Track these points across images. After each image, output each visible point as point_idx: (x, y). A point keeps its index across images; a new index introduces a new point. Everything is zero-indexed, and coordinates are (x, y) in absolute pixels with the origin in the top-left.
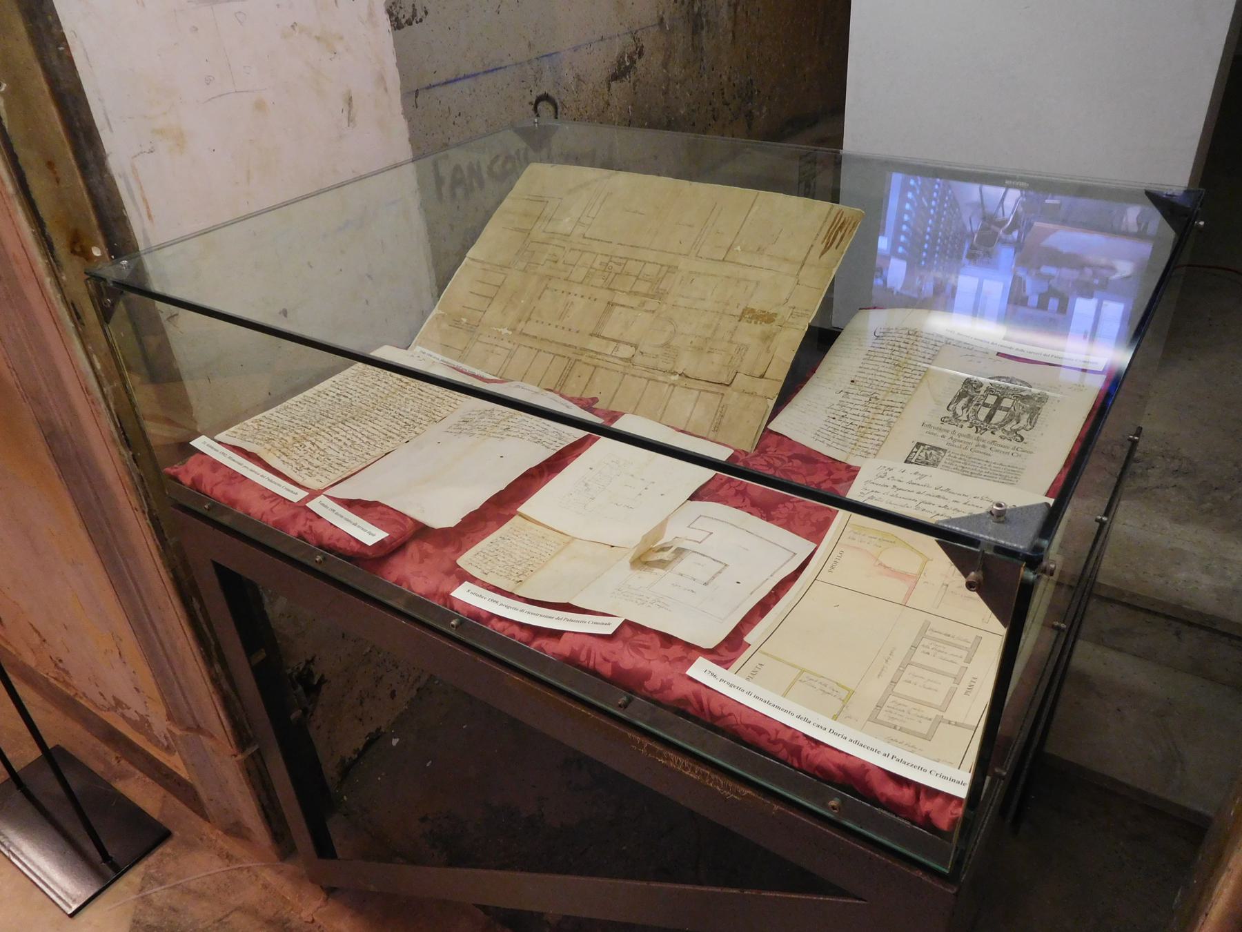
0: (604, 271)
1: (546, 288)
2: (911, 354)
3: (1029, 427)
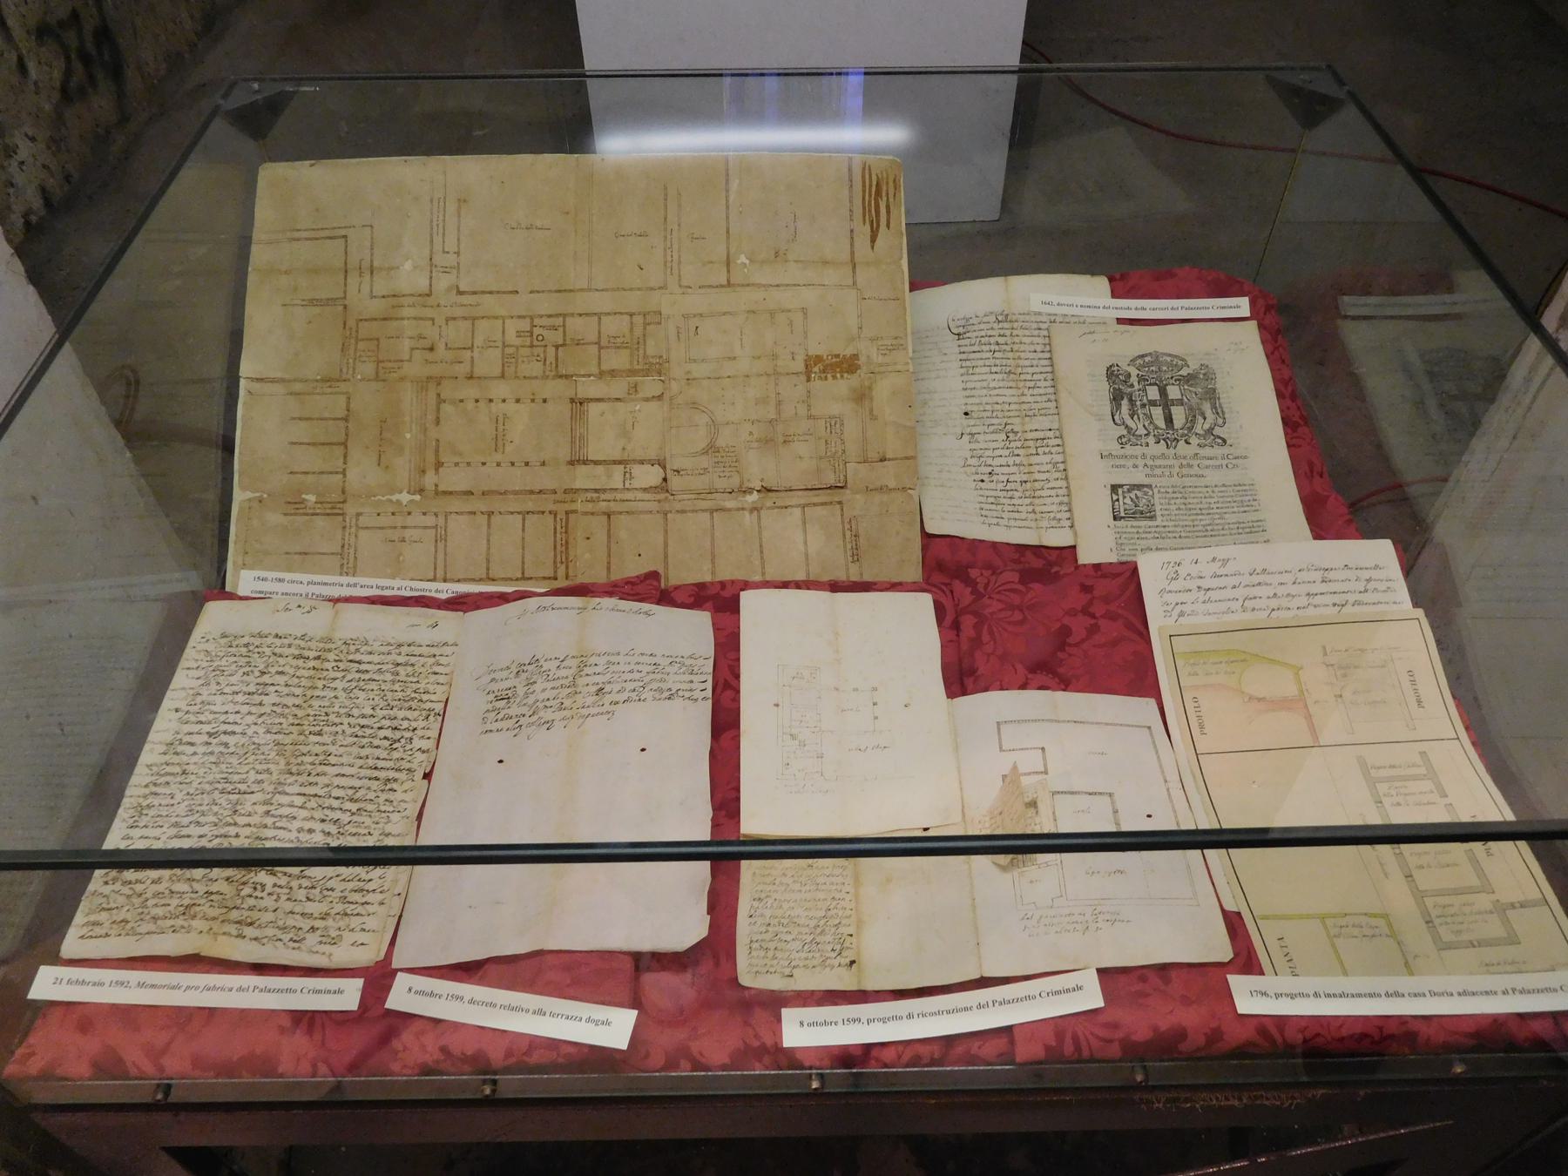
0: (532, 346)
1: (440, 400)
2: (1017, 351)
3: (1220, 421)
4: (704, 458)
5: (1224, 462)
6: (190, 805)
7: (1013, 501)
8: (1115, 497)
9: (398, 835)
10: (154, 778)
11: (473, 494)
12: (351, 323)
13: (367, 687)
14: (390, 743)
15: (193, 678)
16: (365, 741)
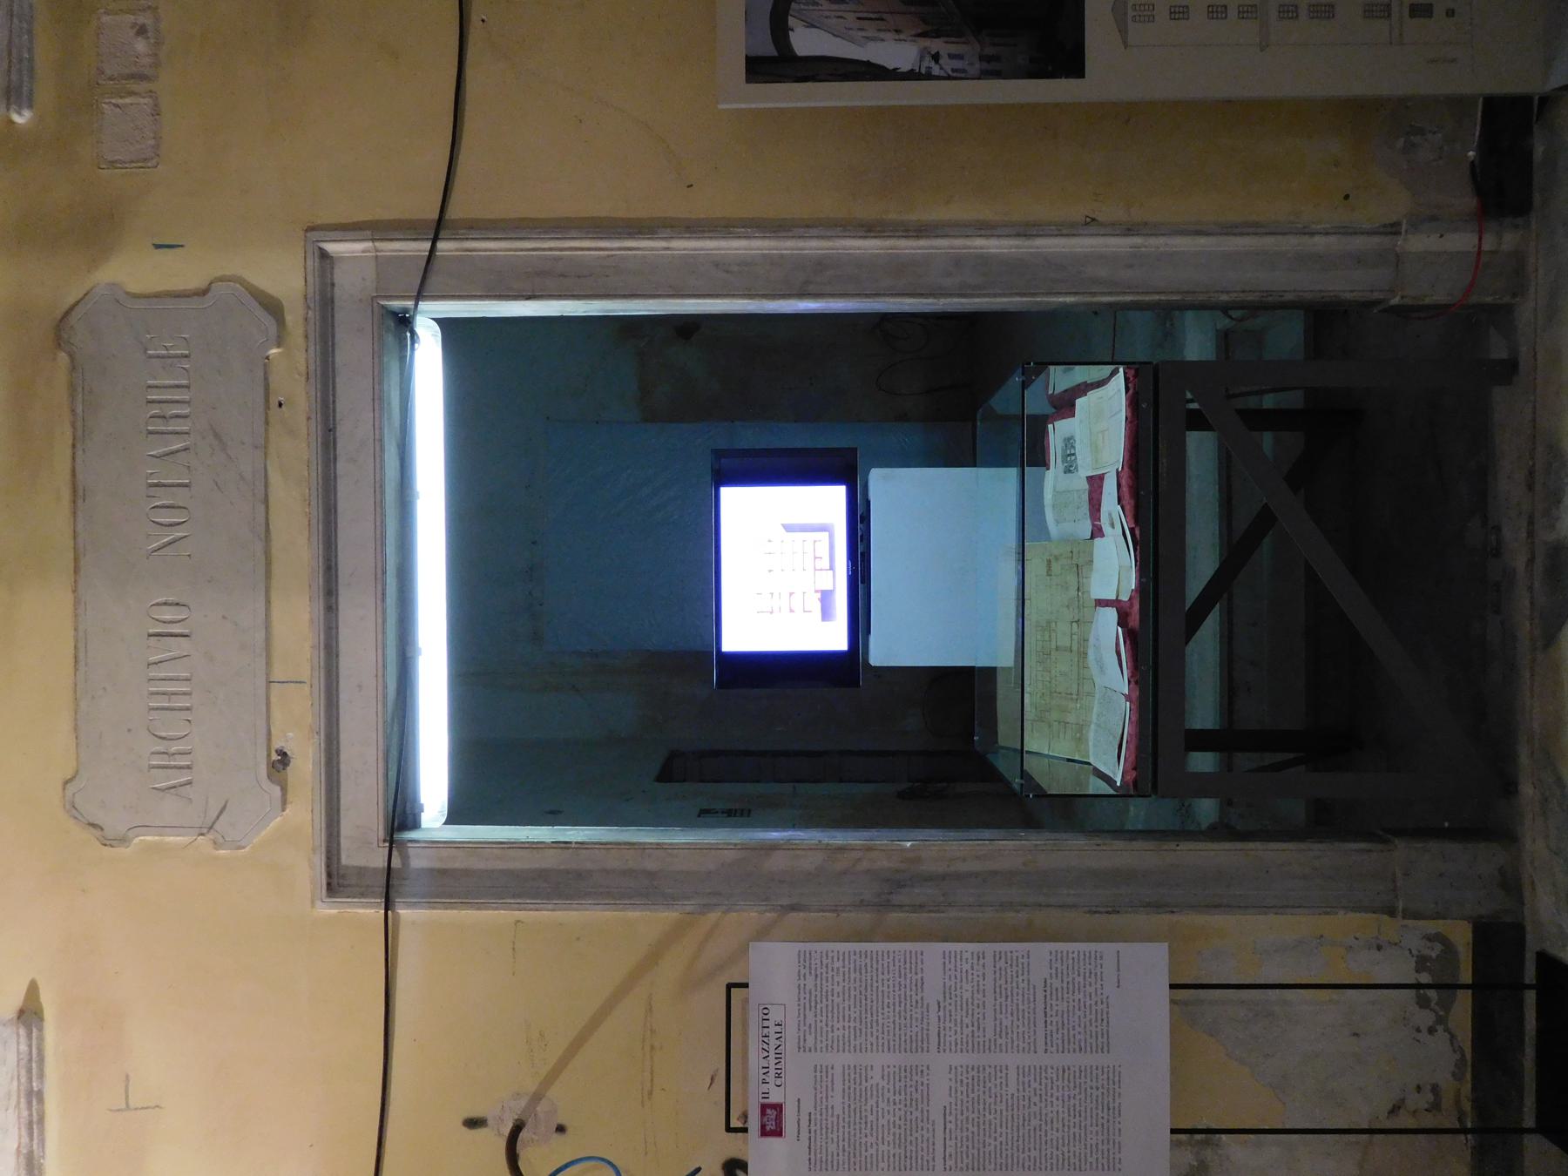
1: (1056, 692)
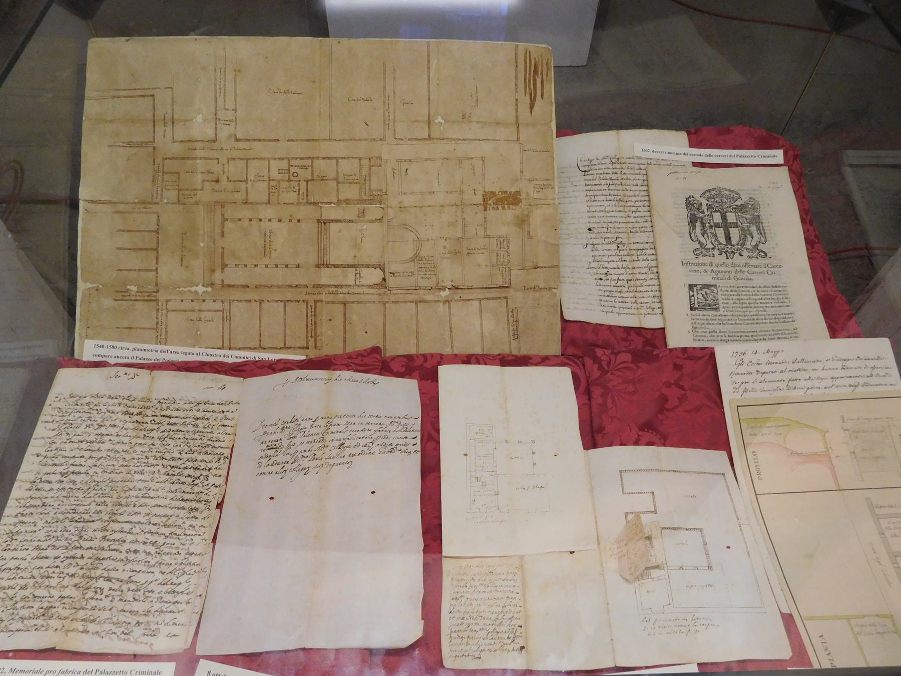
0: (289, 180)
1: (224, 220)
2: (625, 185)
3: (763, 239)
4: (412, 264)
5: (765, 270)
6: (48, 532)
7: (622, 295)
8: (692, 294)
9: (199, 554)
10: (21, 510)
11: (248, 287)
12: (159, 160)
13: (176, 436)
14: (192, 480)
15: (50, 430)
16: (175, 478)
